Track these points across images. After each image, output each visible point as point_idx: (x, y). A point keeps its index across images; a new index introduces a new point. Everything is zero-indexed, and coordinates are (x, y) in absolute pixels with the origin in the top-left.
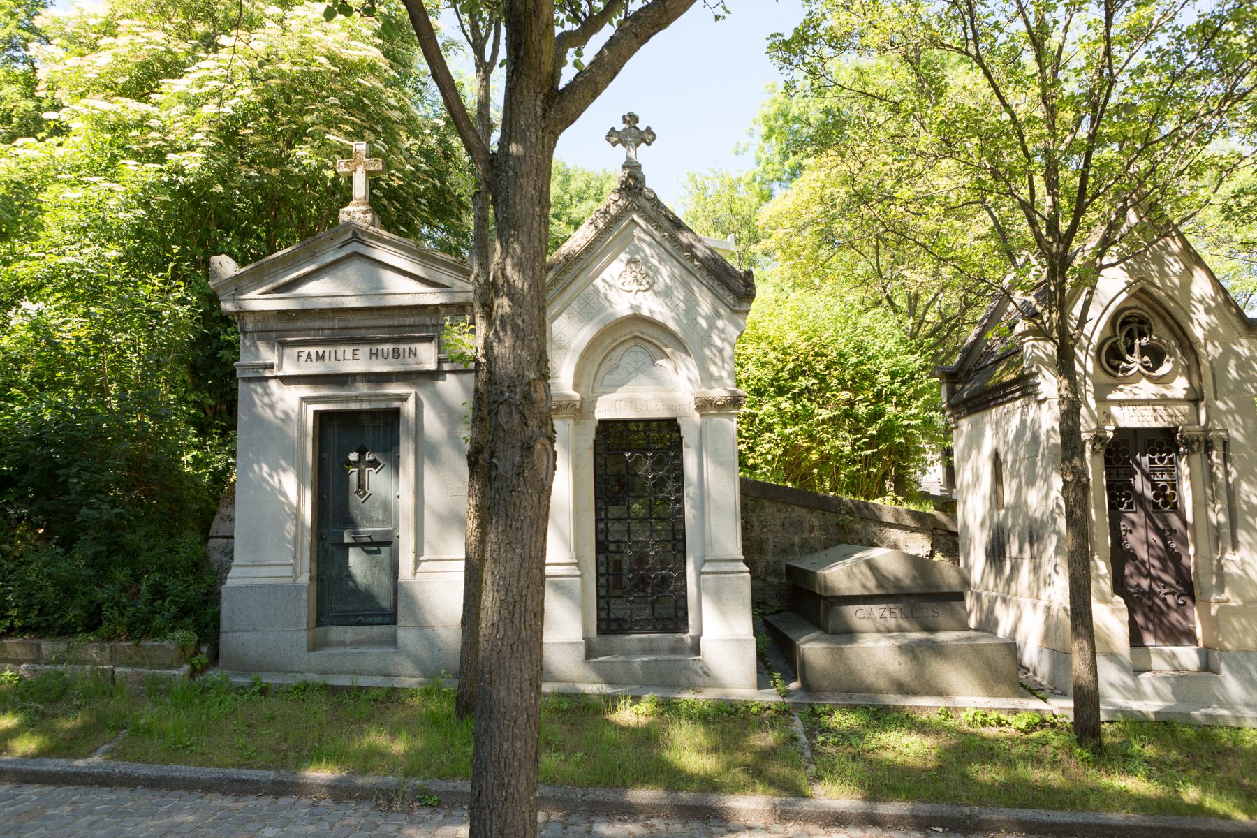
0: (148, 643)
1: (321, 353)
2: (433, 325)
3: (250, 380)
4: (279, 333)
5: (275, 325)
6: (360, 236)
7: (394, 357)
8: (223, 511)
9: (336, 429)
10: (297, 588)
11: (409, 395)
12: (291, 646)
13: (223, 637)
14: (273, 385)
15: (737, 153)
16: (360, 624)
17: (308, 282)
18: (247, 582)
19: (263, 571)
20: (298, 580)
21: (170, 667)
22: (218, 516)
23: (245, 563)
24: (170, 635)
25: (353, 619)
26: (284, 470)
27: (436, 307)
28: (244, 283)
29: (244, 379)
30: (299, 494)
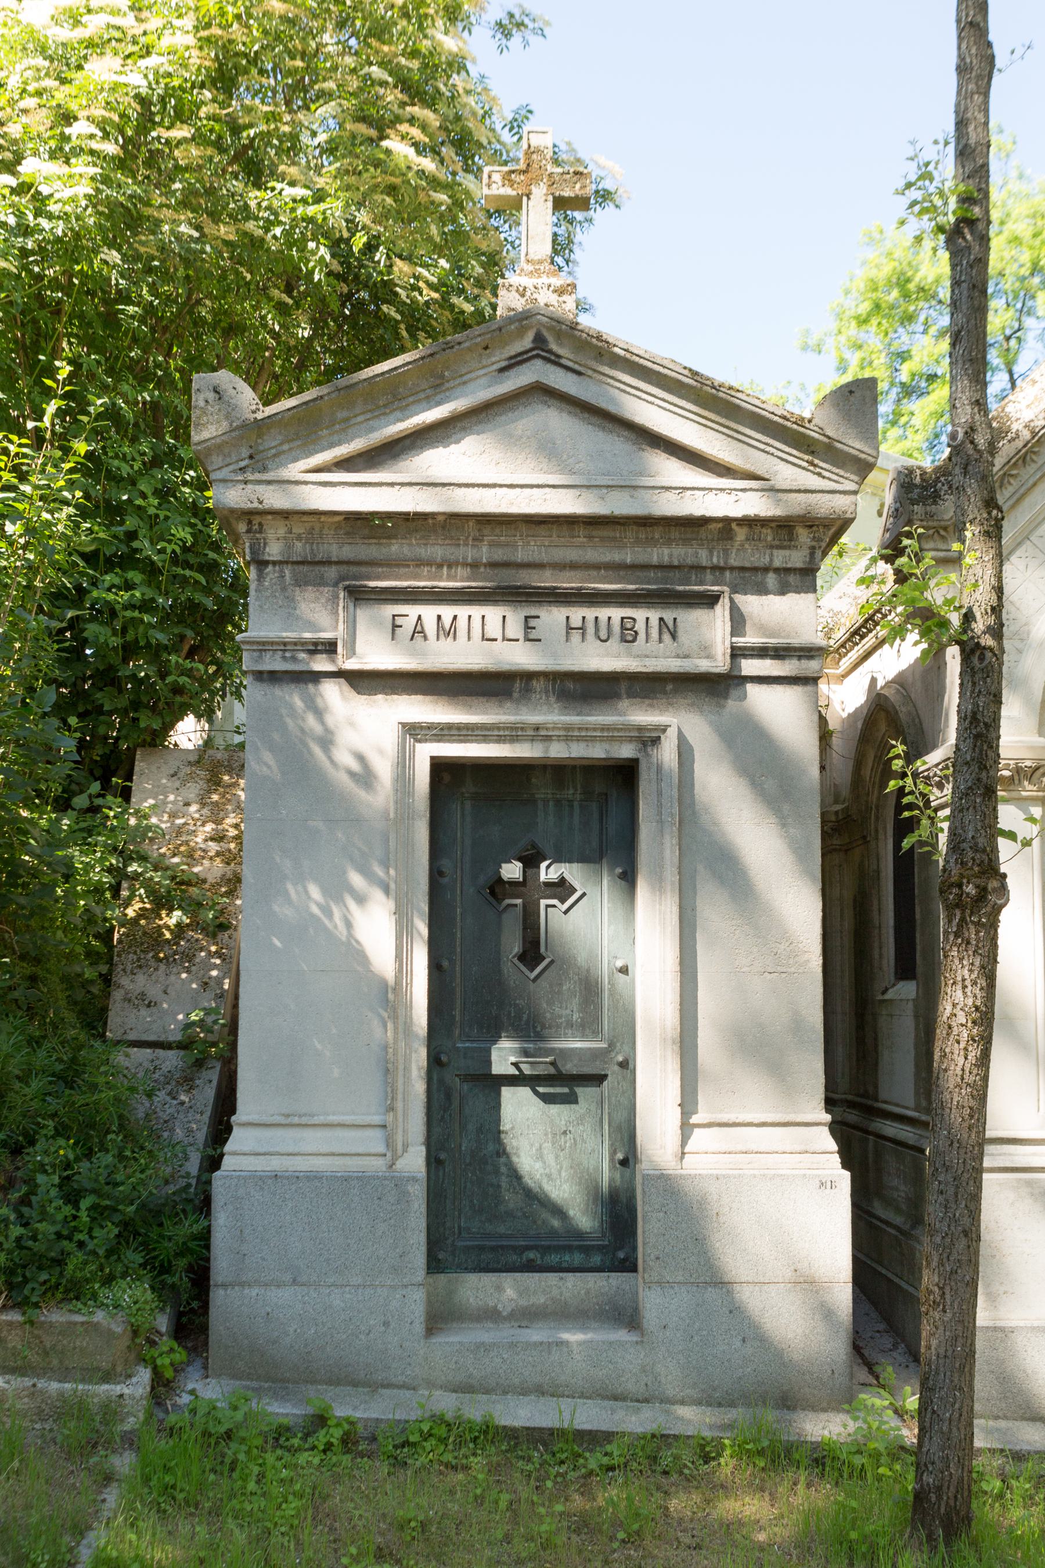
0: (56, 1316)
1: (447, 622)
2: (714, 568)
3: (273, 677)
4: (344, 569)
5: (335, 549)
6: (554, 347)
7: (624, 640)
8: (125, 981)
9: (468, 804)
10: (400, 1183)
11: (664, 729)
12: (386, 1324)
13: (218, 1297)
14: (332, 692)
15: (805, 348)
16: (530, 1267)
17: (422, 448)
18: (275, 1164)
19: (312, 1140)
20: (400, 1164)
21: (107, 1377)
22: (117, 995)
23: (265, 1119)
24: (105, 1294)
25: (513, 1258)
26: (361, 900)
27: (727, 523)
28: (271, 441)
29: (260, 676)
30: (399, 957)
